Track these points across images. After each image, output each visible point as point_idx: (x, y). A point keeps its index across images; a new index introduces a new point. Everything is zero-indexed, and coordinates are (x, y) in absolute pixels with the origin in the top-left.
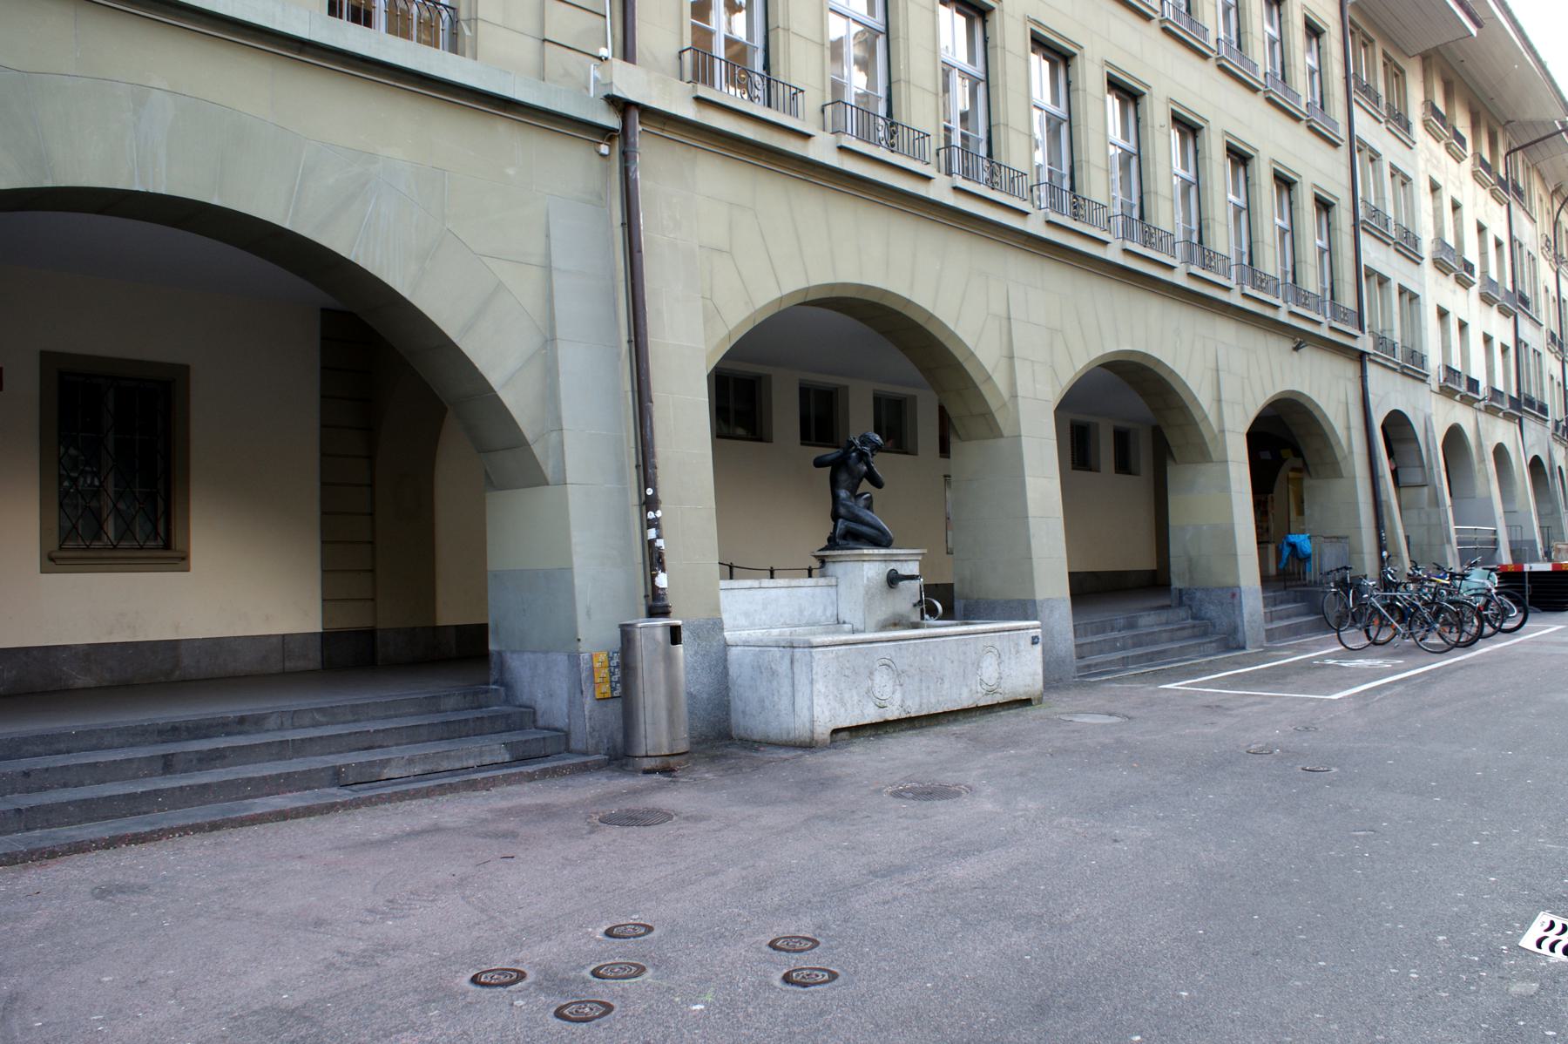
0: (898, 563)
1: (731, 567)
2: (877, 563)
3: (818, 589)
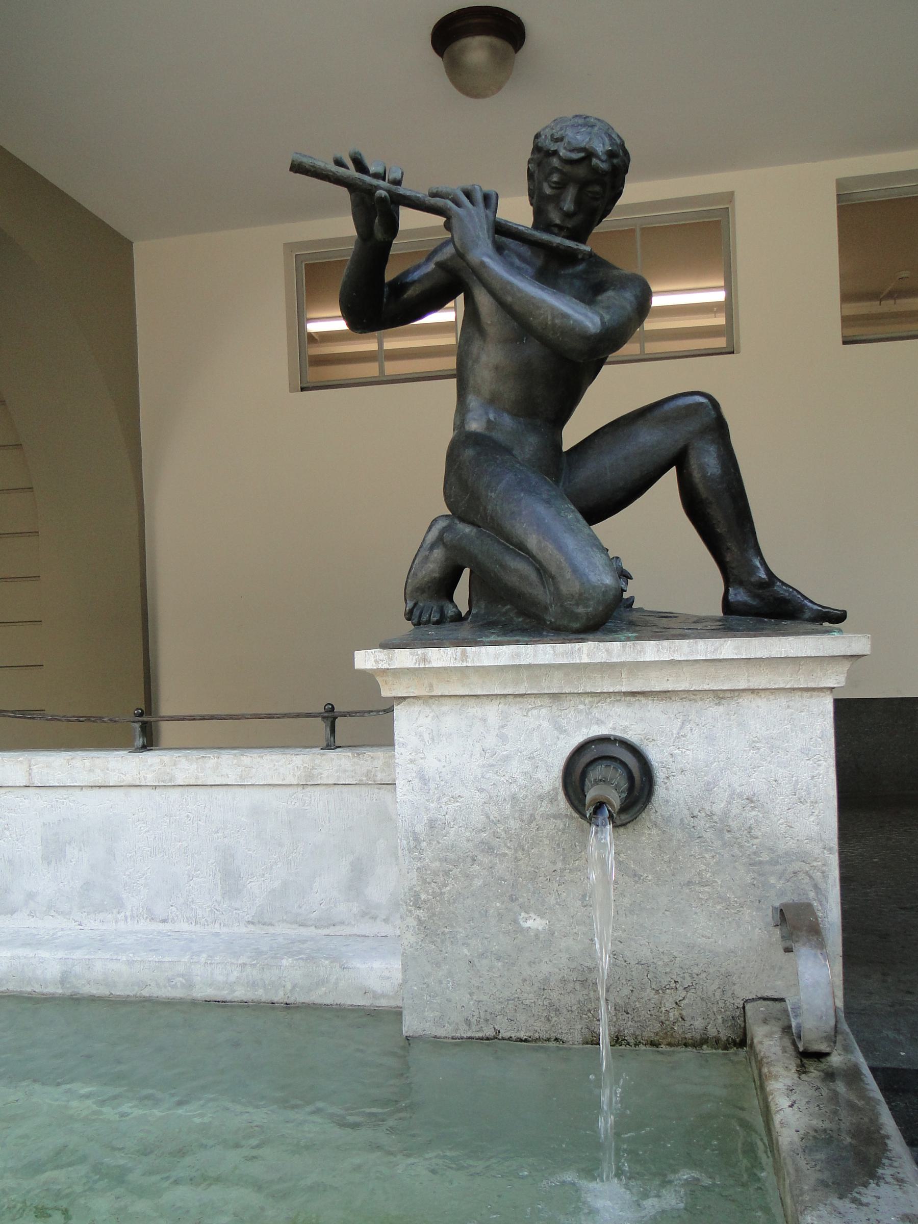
0: (654, 710)
1: (331, 716)
2: (492, 711)
3: (318, 800)
